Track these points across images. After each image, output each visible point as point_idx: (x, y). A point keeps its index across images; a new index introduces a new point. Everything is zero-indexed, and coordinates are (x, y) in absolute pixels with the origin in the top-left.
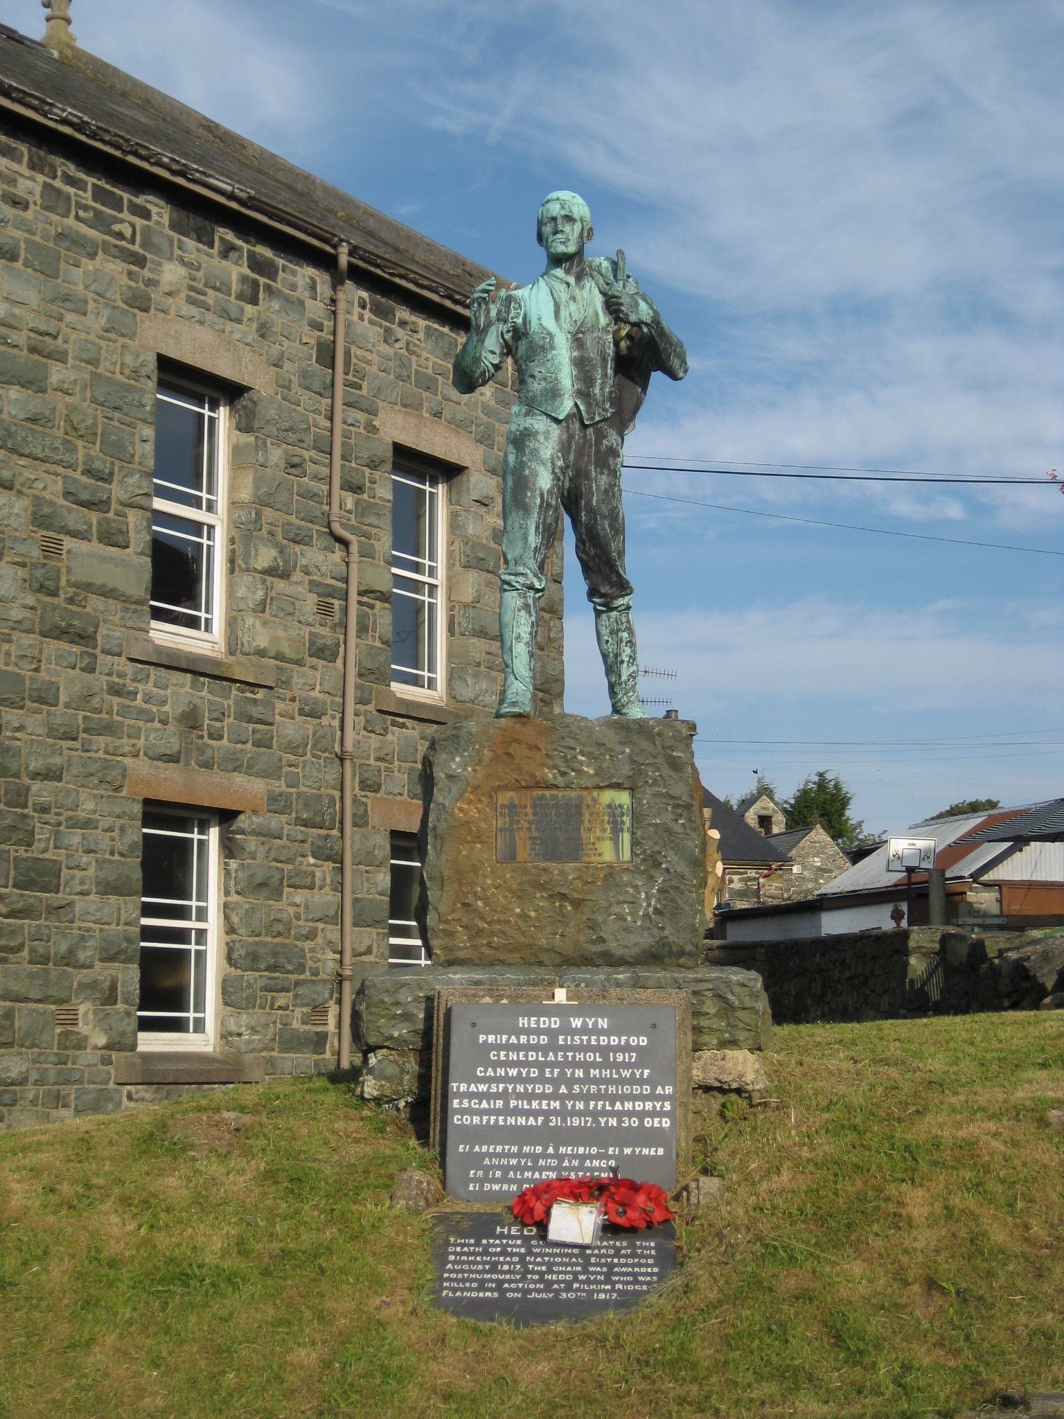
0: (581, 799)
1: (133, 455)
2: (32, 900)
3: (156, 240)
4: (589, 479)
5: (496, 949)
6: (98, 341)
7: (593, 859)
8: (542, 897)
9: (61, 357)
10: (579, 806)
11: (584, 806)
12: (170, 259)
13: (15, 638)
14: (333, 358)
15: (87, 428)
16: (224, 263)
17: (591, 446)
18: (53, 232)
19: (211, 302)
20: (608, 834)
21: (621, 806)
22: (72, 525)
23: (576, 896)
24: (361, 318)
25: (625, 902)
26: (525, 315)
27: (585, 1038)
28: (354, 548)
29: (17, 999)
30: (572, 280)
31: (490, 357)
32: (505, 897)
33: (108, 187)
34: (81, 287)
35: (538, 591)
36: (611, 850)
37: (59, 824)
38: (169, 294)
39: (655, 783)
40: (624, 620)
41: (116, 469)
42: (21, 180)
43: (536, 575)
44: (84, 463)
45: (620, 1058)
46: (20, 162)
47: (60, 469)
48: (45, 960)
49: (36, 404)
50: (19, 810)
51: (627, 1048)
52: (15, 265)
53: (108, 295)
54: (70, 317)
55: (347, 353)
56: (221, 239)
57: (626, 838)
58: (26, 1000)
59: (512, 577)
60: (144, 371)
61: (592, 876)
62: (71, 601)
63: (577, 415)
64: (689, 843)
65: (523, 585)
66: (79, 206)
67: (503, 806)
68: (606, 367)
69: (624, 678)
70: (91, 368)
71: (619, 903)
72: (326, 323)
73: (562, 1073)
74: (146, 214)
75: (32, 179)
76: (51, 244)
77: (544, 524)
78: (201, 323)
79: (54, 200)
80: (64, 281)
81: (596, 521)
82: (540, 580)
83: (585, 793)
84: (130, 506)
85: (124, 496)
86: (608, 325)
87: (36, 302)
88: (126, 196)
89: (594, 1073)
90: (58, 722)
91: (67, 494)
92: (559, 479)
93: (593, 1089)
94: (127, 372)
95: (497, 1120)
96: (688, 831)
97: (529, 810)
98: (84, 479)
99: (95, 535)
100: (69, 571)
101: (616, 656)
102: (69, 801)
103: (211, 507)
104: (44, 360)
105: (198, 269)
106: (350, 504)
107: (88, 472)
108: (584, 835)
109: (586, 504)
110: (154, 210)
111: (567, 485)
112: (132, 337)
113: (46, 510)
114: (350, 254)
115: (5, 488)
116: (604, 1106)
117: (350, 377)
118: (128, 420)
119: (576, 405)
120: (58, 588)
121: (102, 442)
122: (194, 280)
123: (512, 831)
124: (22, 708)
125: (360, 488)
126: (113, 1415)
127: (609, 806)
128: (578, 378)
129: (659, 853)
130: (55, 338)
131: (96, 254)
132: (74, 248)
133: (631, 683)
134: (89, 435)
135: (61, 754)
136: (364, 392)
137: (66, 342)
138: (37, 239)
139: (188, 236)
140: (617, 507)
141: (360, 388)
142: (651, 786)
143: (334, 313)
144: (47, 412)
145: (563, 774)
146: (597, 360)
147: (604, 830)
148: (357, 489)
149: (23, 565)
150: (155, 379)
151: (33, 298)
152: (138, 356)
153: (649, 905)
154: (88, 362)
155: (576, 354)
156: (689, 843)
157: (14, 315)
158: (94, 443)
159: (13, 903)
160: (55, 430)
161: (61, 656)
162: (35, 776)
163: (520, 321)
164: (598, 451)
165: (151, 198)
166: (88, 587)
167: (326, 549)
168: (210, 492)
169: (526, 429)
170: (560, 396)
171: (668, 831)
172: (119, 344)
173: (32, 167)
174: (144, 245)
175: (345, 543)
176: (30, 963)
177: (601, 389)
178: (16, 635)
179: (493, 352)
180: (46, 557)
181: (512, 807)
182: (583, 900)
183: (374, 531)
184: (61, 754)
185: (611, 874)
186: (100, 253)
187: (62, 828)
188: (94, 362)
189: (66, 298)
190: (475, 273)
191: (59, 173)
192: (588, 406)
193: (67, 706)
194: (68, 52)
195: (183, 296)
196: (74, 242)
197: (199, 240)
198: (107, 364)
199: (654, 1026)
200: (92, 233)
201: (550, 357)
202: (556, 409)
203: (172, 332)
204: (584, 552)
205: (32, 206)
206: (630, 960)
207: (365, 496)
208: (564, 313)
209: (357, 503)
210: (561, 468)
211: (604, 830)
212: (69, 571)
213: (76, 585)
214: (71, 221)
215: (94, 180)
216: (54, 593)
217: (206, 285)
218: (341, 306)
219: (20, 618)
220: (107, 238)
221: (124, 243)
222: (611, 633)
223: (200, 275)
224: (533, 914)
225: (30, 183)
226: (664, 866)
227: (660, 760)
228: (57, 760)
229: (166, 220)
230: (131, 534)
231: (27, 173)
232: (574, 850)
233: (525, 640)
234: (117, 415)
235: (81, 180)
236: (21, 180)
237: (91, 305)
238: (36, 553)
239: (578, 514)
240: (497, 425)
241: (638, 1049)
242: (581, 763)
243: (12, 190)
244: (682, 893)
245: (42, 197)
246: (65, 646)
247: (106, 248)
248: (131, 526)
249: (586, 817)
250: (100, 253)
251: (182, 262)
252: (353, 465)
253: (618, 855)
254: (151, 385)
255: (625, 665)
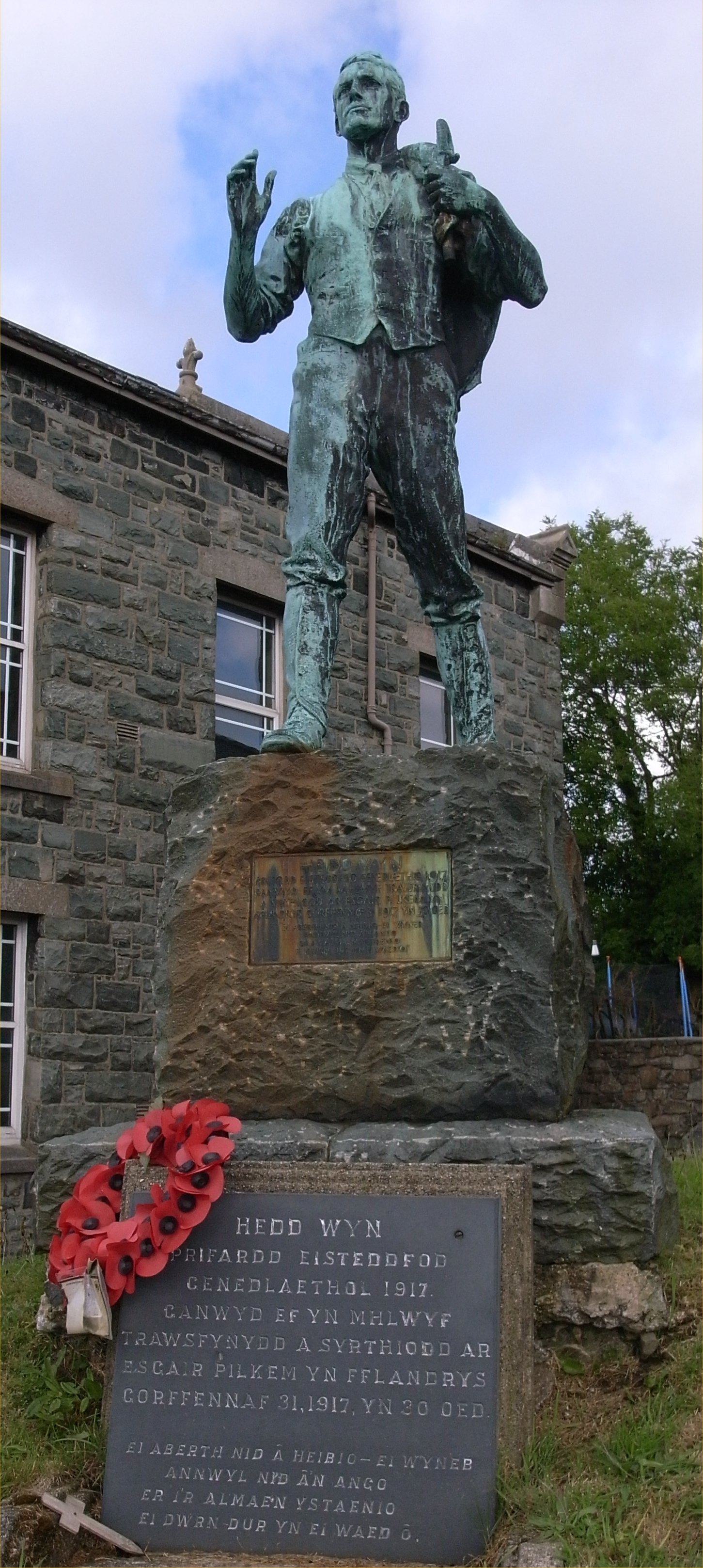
0: (375, 867)
1: (198, 659)
2: (114, 1018)
3: (212, 489)
4: (405, 430)
5: (248, 1095)
6: (163, 568)
7: (393, 955)
8: (317, 1016)
9: (130, 580)
10: (372, 877)
11: (380, 878)
12: (226, 504)
13: (95, 806)
14: (367, 586)
15: (156, 637)
16: (272, 508)
17: (405, 384)
18: (122, 480)
19: (262, 539)
20: (415, 918)
21: (433, 874)
22: (144, 715)
23: (365, 1012)
24: (391, 555)
25: (440, 1021)
26: (313, 220)
27: (343, 1255)
28: (388, 734)
29: (101, 1100)
30: (376, 167)
31: (272, 283)
32: (262, 1017)
33: (170, 446)
34: (148, 525)
35: (333, 585)
36: (426, 942)
37: (138, 956)
38: (226, 532)
39: (487, 838)
40: (470, 635)
41: (183, 670)
42: (92, 437)
43: (328, 563)
44: (154, 665)
45: (402, 1290)
46: (91, 422)
47: (132, 670)
48: (125, 1067)
49: (109, 616)
50: (101, 945)
51: (414, 1274)
52: (89, 505)
53: (172, 531)
54: (139, 548)
55: (379, 583)
56: (270, 490)
57: (441, 924)
58: (110, 1100)
59: (297, 567)
60: (204, 593)
61: (391, 982)
62: (144, 775)
63: (377, 339)
64: (542, 930)
65: (311, 576)
66: (144, 459)
67: (262, 881)
68: (425, 278)
69: (474, 715)
70: (158, 589)
71: (433, 1022)
72: (360, 558)
73: (303, 1317)
74: (204, 469)
75: (102, 436)
76: (121, 490)
77: (340, 492)
78: (255, 556)
79: (122, 455)
80: (133, 519)
81: (418, 491)
82: (336, 570)
83: (380, 858)
84: (196, 700)
85: (190, 692)
86: (426, 219)
87: (109, 535)
88: (186, 454)
89: (358, 1319)
90: (134, 873)
91: (140, 690)
92: (360, 431)
93: (355, 1346)
94: (190, 593)
95: (191, 1399)
96: (540, 910)
97: (298, 885)
98: (154, 678)
99: (165, 724)
100: (142, 751)
101: (462, 685)
102: (145, 937)
103: (269, 703)
104: (117, 582)
105: (251, 513)
106: (384, 701)
107: (159, 672)
108: (379, 919)
109: (403, 468)
110: (211, 465)
111: (375, 441)
112: (194, 565)
113: (121, 703)
114: (378, 502)
115: (85, 684)
116: (372, 1377)
117: (382, 601)
118: (191, 631)
119: (380, 324)
120: (133, 765)
121: (169, 649)
122: (247, 521)
123: (273, 918)
124: (103, 862)
125: (392, 687)
126: (695, 1091)
127: (418, 875)
128: (382, 289)
129: (494, 944)
130: (126, 564)
131: (160, 498)
132: (141, 494)
133: (484, 720)
134: (158, 643)
135: (138, 899)
136: (394, 613)
137: (135, 568)
138: (109, 484)
139: (240, 487)
140: (448, 473)
141: (391, 609)
142: (479, 843)
143: (367, 550)
144: (120, 624)
145: (349, 830)
146: (411, 266)
147: (411, 912)
148: (390, 688)
149: (102, 747)
150: (215, 599)
151: (105, 532)
152: (199, 580)
153: (479, 1025)
154: (156, 585)
155: (379, 256)
156: (542, 930)
157: (89, 545)
158: (163, 650)
159: (96, 1021)
160: (128, 638)
161: (136, 820)
162: (116, 917)
163: (307, 226)
164: (416, 392)
165: (208, 456)
166: (160, 764)
167: (365, 734)
168: (269, 691)
169: (314, 366)
170: (357, 313)
171: (507, 909)
172: (183, 571)
173: (103, 427)
174: (202, 493)
175: (381, 731)
176: (112, 1069)
177: (418, 306)
178: (96, 804)
179: (275, 278)
180: (121, 740)
181: (273, 880)
182: (378, 1019)
183: (405, 721)
184: (138, 899)
185: (421, 983)
186: (165, 498)
187: (140, 959)
188: (161, 584)
189: (136, 533)
190: (489, 529)
191: (127, 433)
192: (399, 325)
193: (143, 860)
194: (196, 398)
195: (238, 534)
196: (141, 488)
197: (251, 490)
198: (173, 586)
199: (459, 1234)
200: (156, 481)
201: (343, 264)
202: (353, 332)
203: (229, 562)
204: (409, 541)
205: (103, 458)
206: (450, 1110)
207: (397, 694)
208: (363, 205)
209: (390, 699)
210: (362, 415)
211: (411, 912)
212: (142, 751)
213: (148, 763)
214: (138, 471)
215: (158, 440)
216: (129, 770)
217: (257, 525)
218: (373, 544)
219: (99, 789)
220: (171, 486)
221: (185, 491)
222: (454, 655)
223: (252, 517)
224: (303, 1041)
225: (100, 441)
226: (502, 964)
227: (492, 803)
228: (135, 904)
229: (222, 473)
230: (198, 721)
231: (99, 432)
232: (366, 943)
233: (314, 652)
234: (183, 627)
235: (146, 439)
236: (92, 437)
237: (158, 539)
238: (114, 737)
239: (395, 483)
240: (505, 641)
241: (430, 1275)
242: (376, 812)
243: (85, 445)
244: (531, 1005)
245: (111, 451)
246: (141, 812)
247: (169, 494)
248: (197, 717)
249: (383, 894)
250: (165, 498)
251: (237, 508)
252: (387, 669)
253: (430, 950)
254: (212, 604)
255: (475, 697)
